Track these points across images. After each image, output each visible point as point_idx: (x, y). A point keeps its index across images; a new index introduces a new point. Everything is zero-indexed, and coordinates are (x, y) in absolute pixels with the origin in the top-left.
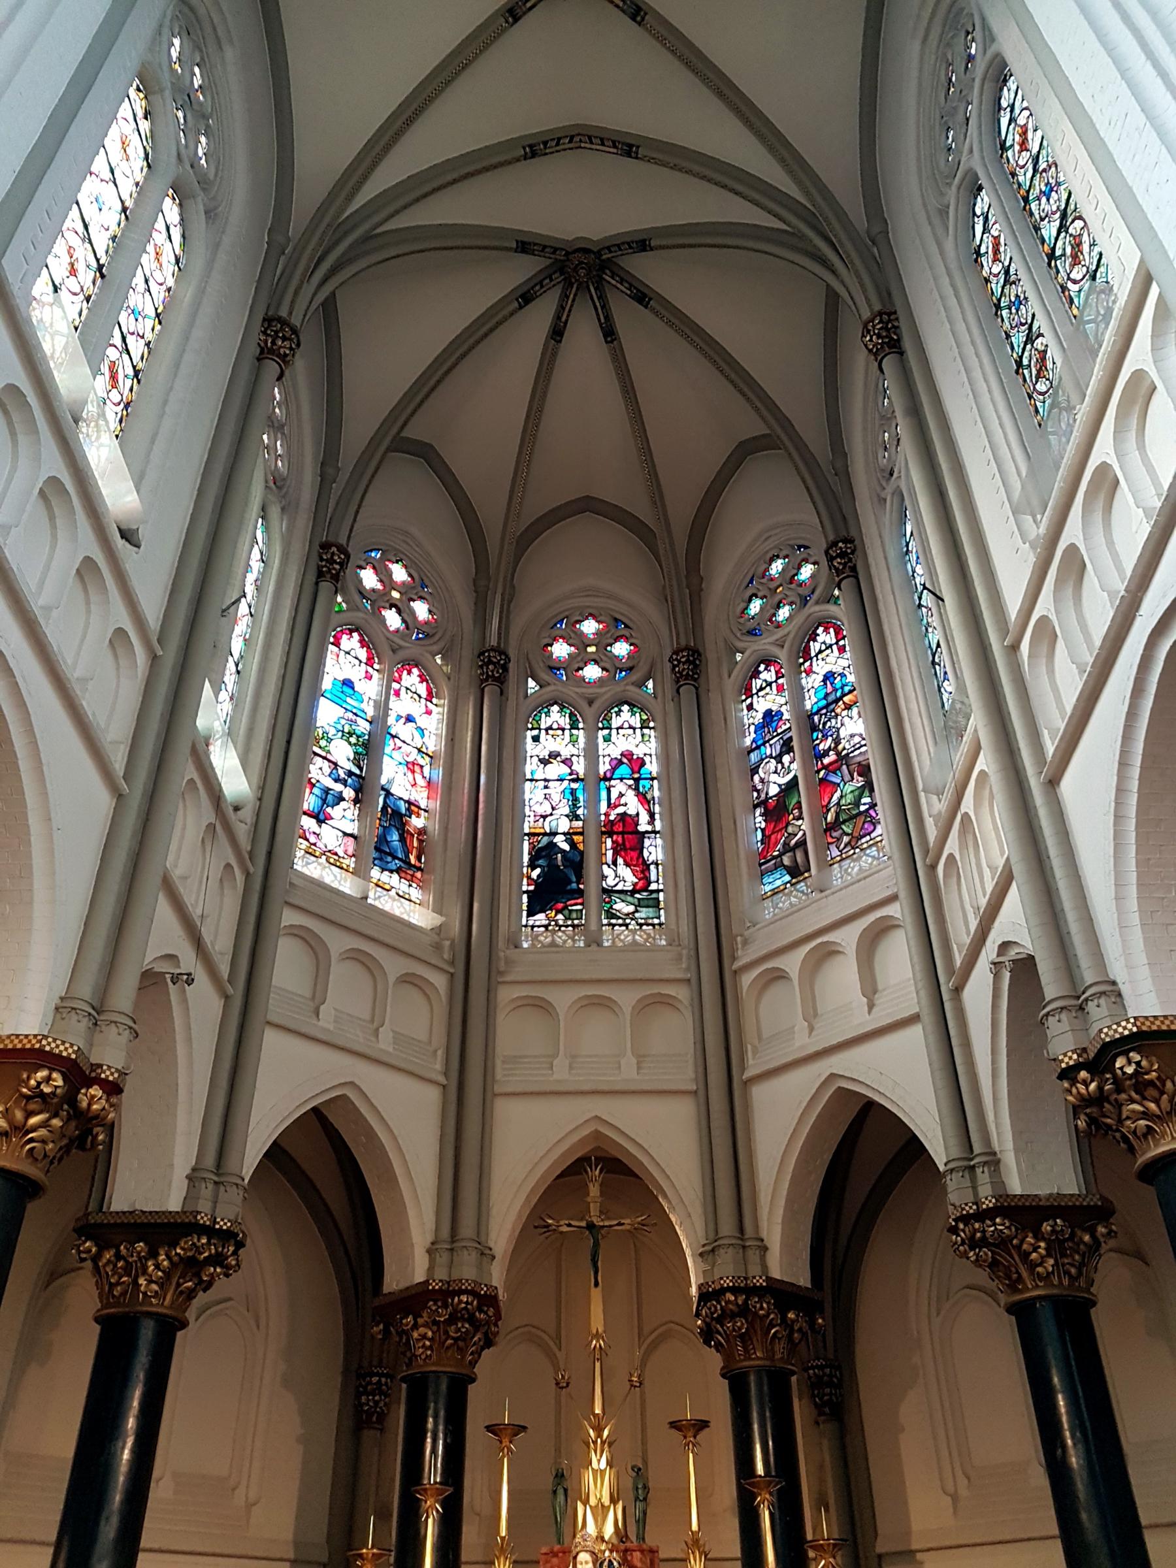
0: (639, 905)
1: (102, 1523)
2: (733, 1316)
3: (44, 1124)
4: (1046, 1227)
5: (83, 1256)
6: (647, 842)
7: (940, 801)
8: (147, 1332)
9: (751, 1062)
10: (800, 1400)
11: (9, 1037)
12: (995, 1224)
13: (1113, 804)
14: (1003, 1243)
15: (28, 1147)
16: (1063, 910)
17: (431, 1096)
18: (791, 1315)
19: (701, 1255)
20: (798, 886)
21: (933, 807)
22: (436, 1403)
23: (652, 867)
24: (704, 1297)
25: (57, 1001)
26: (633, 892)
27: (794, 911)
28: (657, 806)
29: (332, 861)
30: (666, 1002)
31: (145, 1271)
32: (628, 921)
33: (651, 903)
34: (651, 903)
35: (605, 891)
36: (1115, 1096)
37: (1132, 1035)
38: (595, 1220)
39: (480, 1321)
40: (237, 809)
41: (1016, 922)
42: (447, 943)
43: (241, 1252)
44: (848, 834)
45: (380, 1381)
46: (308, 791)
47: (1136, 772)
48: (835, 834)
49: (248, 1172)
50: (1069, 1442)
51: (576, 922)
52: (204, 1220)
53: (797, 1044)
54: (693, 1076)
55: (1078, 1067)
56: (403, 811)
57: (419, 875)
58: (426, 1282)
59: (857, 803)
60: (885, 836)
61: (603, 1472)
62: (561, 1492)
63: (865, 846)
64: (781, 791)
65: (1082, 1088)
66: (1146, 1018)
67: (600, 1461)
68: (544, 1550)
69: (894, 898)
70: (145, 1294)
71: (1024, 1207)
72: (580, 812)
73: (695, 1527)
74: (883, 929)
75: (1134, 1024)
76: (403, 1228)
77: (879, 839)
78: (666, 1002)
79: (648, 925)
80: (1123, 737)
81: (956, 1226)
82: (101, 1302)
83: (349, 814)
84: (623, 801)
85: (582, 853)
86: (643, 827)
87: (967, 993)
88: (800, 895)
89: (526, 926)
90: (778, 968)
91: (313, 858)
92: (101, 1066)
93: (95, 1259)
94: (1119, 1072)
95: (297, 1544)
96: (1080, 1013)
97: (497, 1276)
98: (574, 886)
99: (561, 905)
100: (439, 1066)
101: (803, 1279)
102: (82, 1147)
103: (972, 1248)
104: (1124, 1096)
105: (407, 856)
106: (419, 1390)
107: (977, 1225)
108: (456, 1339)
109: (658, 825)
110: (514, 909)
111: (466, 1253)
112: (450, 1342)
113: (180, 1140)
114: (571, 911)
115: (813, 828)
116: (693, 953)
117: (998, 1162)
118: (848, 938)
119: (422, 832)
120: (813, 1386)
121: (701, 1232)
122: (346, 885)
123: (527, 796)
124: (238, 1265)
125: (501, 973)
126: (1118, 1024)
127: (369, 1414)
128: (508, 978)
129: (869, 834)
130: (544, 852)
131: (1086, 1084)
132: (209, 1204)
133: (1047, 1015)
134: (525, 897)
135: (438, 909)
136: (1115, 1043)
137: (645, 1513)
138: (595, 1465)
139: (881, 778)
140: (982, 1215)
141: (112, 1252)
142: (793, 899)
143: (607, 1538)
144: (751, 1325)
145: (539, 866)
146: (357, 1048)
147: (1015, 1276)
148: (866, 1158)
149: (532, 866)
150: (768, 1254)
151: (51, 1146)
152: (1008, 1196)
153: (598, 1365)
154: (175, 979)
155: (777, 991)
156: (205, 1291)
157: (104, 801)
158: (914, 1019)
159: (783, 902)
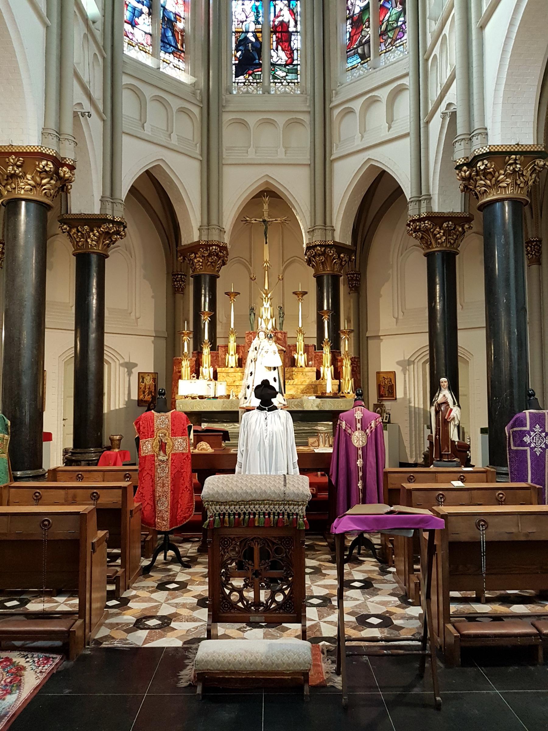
0: (288, 72)
1: (91, 322)
2: (319, 255)
3: (48, 183)
4: (445, 225)
5: (64, 231)
6: (293, 38)
7: (436, 24)
8: (94, 259)
9: (335, 152)
10: (344, 285)
11: (27, 147)
12: (425, 223)
13: (503, 45)
14: (427, 230)
15: (44, 192)
16: (473, 93)
17: (196, 165)
18: (342, 255)
19: (308, 232)
20: (364, 65)
21: (432, 27)
22: (205, 285)
23: (295, 52)
24: (308, 248)
25: (41, 130)
26: (286, 65)
27: (360, 78)
28: (299, 16)
29: (141, 48)
30: (299, 122)
31: (89, 237)
32: (283, 81)
33: (294, 71)
34: (294, 71)
35: (272, 64)
36: (475, 177)
37: (487, 153)
38: (266, 218)
39: (220, 256)
40: (94, 22)
41: (454, 95)
42: (199, 91)
43: (126, 229)
44: (390, 38)
45: (181, 277)
46: (125, 9)
47: (516, 29)
48: (384, 37)
49: (124, 198)
50: (438, 301)
51: (258, 81)
52: (110, 217)
53: (356, 144)
54: (309, 157)
55: (464, 165)
56: (173, 19)
57: (182, 55)
58: (199, 242)
59: (397, 21)
60: (408, 40)
61: (268, 309)
62: (252, 314)
63: (398, 45)
64: (361, 11)
65: (463, 174)
66: (494, 146)
67: (267, 305)
68: (247, 332)
69: (407, 75)
70: (91, 245)
71: (438, 217)
72: (260, 19)
73: (300, 326)
74: (400, 90)
75: (489, 148)
76: (188, 221)
77: (405, 41)
78: (299, 122)
79: (292, 83)
80: (514, 10)
81: (410, 224)
82: (74, 248)
83: (146, 21)
84: (282, 13)
85: (261, 43)
86: (292, 29)
87: (431, 125)
88: (364, 69)
89: (235, 82)
90: (351, 108)
91: (131, 47)
92: (65, 158)
93: (69, 232)
94: (478, 168)
95: (155, 331)
96: (469, 142)
97: (226, 239)
98: (257, 61)
99: (251, 72)
100: (198, 151)
101: (348, 242)
102: (63, 191)
103: (414, 232)
104: (478, 177)
105: (176, 45)
106: (198, 280)
107: (418, 224)
108: (212, 262)
109: (299, 28)
110: (229, 74)
111: (214, 230)
112: (209, 263)
113: (95, 184)
114: (255, 75)
115: (374, 33)
116: (312, 99)
117: (431, 199)
118: (384, 94)
119: (183, 31)
120: (349, 281)
121: (309, 223)
122: (148, 60)
123: (233, 10)
124: (125, 235)
125: (224, 107)
126: (482, 148)
127: (178, 288)
128: (227, 109)
129: (401, 38)
130: (242, 43)
131: (465, 172)
132: (111, 211)
133: (456, 142)
134: (234, 67)
135: (193, 74)
136: (479, 156)
137: (283, 321)
138: (265, 306)
139: (410, 9)
140: (420, 220)
141: (75, 229)
142: (361, 72)
143: (269, 329)
144: (326, 258)
145: (240, 50)
146: (162, 143)
147: (429, 243)
148: (379, 195)
149: (237, 50)
150: (335, 232)
151: (52, 191)
152: (432, 212)
153: (266, 272)
154: (83, 115)
155: (348, 118)
156: (113, 244)
157: (41, 30)
158: (407, 135)
159: (356, 73)
